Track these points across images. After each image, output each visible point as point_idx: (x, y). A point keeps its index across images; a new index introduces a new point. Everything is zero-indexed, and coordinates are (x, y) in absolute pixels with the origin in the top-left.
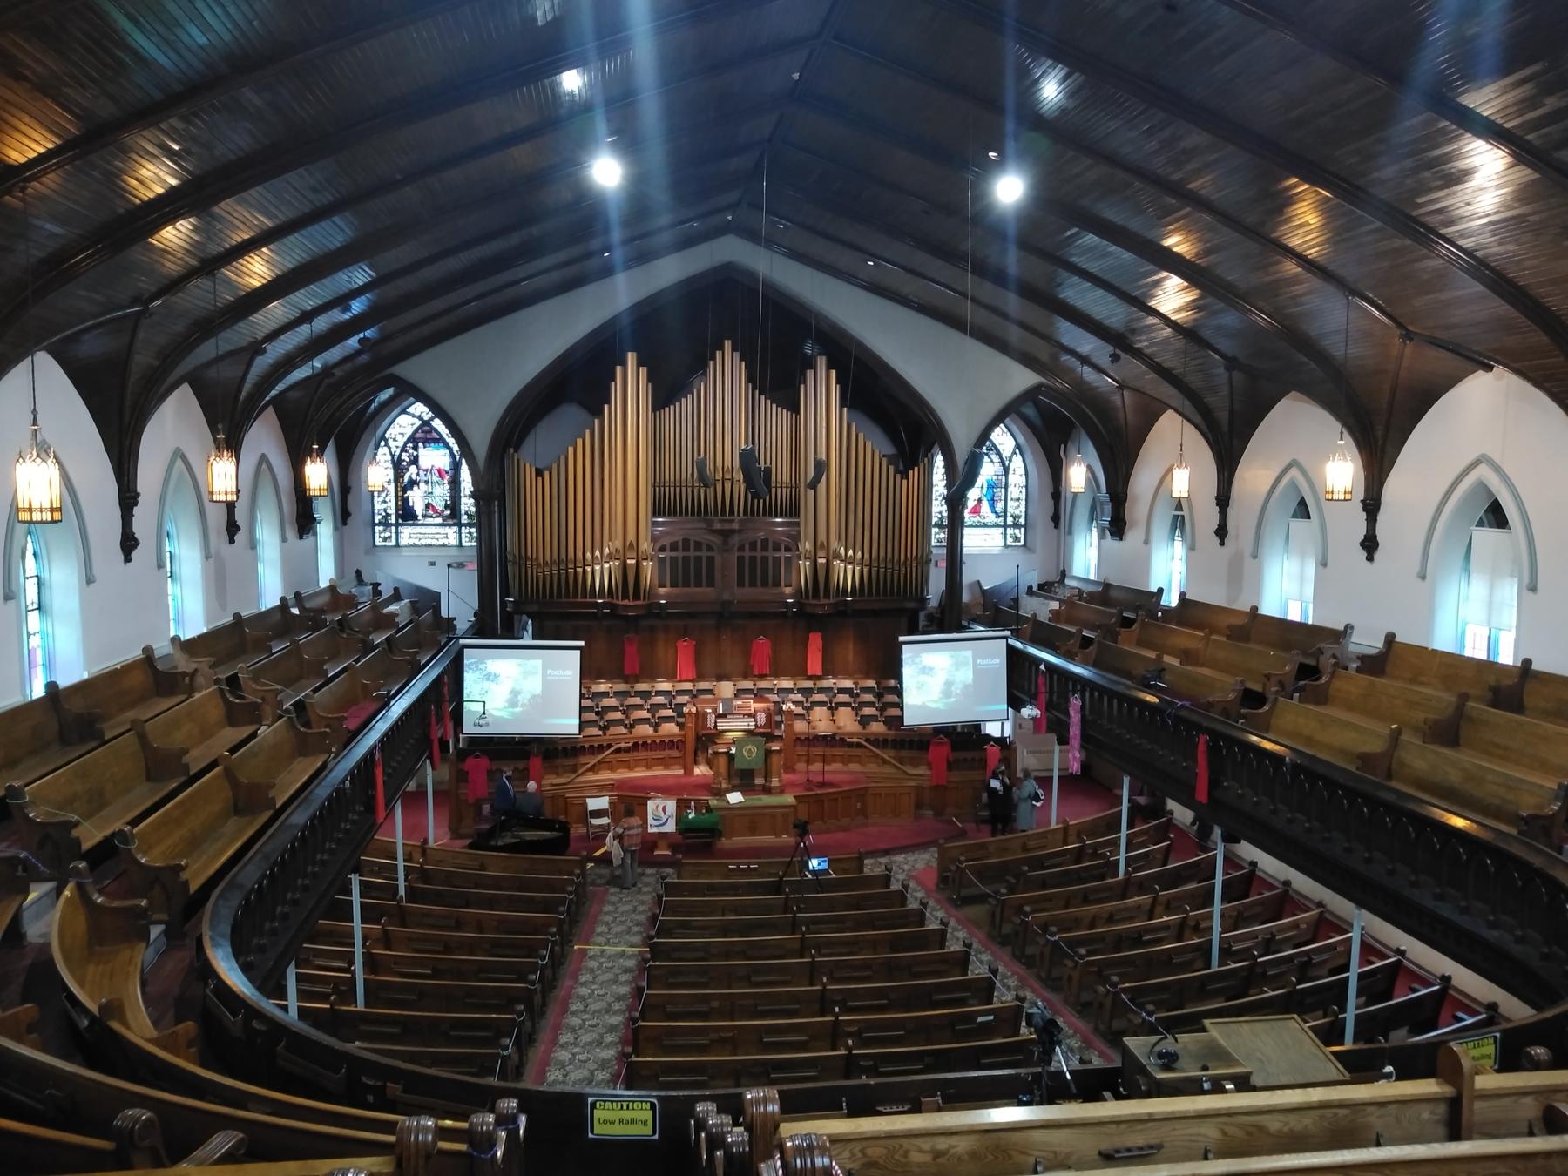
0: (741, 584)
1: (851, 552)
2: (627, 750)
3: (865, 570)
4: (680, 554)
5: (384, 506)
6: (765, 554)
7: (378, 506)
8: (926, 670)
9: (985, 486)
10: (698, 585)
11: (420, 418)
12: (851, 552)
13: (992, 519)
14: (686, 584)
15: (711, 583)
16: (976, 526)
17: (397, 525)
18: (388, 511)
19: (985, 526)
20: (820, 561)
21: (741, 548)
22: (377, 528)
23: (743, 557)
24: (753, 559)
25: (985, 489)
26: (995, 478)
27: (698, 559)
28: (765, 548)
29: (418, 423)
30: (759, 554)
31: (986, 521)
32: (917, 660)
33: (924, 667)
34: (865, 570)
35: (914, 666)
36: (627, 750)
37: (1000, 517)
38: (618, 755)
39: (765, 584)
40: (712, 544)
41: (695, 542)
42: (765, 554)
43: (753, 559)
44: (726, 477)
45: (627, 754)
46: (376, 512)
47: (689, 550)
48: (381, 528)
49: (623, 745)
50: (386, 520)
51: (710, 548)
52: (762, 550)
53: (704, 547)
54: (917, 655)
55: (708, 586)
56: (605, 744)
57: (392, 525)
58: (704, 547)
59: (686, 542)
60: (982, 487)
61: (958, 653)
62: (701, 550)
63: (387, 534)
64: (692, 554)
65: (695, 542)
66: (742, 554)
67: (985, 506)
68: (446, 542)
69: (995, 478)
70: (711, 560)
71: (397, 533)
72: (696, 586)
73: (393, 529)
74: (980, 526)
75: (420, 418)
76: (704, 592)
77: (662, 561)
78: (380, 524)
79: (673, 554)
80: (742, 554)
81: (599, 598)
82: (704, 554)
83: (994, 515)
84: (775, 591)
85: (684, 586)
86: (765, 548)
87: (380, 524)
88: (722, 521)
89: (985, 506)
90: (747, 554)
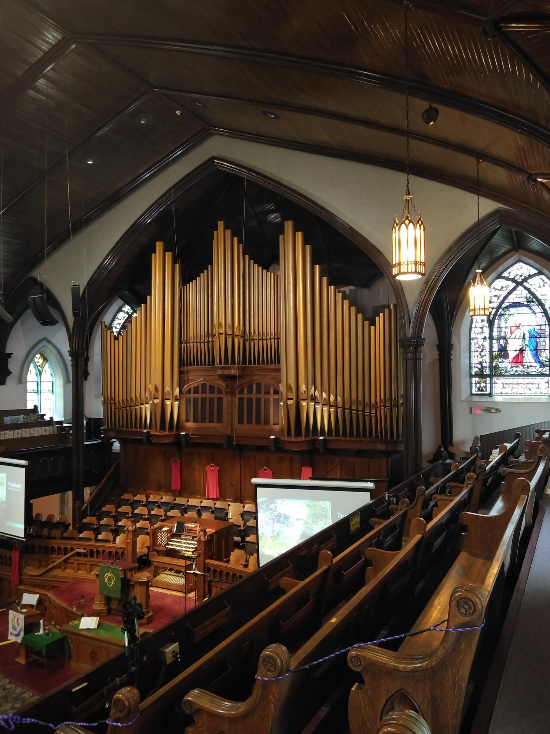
0: (241, 421)
1: (324, 395)
2: (85, 555)
3: (339, 411)
4: (199, 396)
5: (480, 360)
6: (259, 396)
7: (474, 360)
8: (282, 519)
9: (527, 336)
10: (211, 421)
11: (127, 313)
12: (324, 395)
13: (536, 368)
14: (203, 421)
15: (220, 420)
16: (519, 375)
17: (490, 376)
18: (484, 364)
19: (528, 375)
20: (290, 402)
21: (241, 392)
22: (474, 380)
23: (243, 398)
24: (250, 400)
25: (527, 340)
26: (538, 328)
27: (212, 400)
28: (259, 392)
29: (126, 316)
30: (254, 396)
31: (530, 369)
32: (272, 506)
33: (279, 515)
34: (339, 411)
35: (269, 512)
36: (85, 555)
37: (544, 366)
38: (79, 558)
39: (258, 422)
40: (221, 388)
41: (210, 386)
42: (259, 396)
43: (250, 400)
44: (272, 338)
45: (85, 559)
46: (473, 365)
47: (205, 393)
48: (477, 379)
49: (82, 551)
50: (482, 372)
51: (220, 391)
52: (257, 393)
53: (216, 390)
54: (271, 500)
55: (218, 422)
56: (69, 547)
57: (487, 376)
58: (216, 390)
59: (204, 386)
60: (524, 338)
61: (314, 503)
62: (213, 393)
63: (483, 385)
64: (208, 396)
65: (210, 386)
66: (241, 396)
67: (528, 357)
68: (538, 391)
69: (538, 328)
70: (220, 400)
71: (491, 383)
72: (210, 422)
73: (488, 379)
74: (523, 376)
75: (127, 313)
76: (214, 425)
77: (188, 400)
78: (476, 375)
79: (196, 396)
80: (241, 396)
81: (321, 436)
82: (216, 396)
83: (537, 365)
84: (266, 427)
85: (202, 422)
86: (259, 392)
87: (476, 375)
88: (222, 368)
89: (528, 357)
90: (245, 396)
